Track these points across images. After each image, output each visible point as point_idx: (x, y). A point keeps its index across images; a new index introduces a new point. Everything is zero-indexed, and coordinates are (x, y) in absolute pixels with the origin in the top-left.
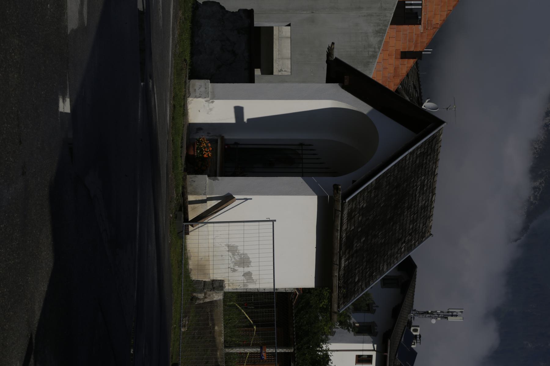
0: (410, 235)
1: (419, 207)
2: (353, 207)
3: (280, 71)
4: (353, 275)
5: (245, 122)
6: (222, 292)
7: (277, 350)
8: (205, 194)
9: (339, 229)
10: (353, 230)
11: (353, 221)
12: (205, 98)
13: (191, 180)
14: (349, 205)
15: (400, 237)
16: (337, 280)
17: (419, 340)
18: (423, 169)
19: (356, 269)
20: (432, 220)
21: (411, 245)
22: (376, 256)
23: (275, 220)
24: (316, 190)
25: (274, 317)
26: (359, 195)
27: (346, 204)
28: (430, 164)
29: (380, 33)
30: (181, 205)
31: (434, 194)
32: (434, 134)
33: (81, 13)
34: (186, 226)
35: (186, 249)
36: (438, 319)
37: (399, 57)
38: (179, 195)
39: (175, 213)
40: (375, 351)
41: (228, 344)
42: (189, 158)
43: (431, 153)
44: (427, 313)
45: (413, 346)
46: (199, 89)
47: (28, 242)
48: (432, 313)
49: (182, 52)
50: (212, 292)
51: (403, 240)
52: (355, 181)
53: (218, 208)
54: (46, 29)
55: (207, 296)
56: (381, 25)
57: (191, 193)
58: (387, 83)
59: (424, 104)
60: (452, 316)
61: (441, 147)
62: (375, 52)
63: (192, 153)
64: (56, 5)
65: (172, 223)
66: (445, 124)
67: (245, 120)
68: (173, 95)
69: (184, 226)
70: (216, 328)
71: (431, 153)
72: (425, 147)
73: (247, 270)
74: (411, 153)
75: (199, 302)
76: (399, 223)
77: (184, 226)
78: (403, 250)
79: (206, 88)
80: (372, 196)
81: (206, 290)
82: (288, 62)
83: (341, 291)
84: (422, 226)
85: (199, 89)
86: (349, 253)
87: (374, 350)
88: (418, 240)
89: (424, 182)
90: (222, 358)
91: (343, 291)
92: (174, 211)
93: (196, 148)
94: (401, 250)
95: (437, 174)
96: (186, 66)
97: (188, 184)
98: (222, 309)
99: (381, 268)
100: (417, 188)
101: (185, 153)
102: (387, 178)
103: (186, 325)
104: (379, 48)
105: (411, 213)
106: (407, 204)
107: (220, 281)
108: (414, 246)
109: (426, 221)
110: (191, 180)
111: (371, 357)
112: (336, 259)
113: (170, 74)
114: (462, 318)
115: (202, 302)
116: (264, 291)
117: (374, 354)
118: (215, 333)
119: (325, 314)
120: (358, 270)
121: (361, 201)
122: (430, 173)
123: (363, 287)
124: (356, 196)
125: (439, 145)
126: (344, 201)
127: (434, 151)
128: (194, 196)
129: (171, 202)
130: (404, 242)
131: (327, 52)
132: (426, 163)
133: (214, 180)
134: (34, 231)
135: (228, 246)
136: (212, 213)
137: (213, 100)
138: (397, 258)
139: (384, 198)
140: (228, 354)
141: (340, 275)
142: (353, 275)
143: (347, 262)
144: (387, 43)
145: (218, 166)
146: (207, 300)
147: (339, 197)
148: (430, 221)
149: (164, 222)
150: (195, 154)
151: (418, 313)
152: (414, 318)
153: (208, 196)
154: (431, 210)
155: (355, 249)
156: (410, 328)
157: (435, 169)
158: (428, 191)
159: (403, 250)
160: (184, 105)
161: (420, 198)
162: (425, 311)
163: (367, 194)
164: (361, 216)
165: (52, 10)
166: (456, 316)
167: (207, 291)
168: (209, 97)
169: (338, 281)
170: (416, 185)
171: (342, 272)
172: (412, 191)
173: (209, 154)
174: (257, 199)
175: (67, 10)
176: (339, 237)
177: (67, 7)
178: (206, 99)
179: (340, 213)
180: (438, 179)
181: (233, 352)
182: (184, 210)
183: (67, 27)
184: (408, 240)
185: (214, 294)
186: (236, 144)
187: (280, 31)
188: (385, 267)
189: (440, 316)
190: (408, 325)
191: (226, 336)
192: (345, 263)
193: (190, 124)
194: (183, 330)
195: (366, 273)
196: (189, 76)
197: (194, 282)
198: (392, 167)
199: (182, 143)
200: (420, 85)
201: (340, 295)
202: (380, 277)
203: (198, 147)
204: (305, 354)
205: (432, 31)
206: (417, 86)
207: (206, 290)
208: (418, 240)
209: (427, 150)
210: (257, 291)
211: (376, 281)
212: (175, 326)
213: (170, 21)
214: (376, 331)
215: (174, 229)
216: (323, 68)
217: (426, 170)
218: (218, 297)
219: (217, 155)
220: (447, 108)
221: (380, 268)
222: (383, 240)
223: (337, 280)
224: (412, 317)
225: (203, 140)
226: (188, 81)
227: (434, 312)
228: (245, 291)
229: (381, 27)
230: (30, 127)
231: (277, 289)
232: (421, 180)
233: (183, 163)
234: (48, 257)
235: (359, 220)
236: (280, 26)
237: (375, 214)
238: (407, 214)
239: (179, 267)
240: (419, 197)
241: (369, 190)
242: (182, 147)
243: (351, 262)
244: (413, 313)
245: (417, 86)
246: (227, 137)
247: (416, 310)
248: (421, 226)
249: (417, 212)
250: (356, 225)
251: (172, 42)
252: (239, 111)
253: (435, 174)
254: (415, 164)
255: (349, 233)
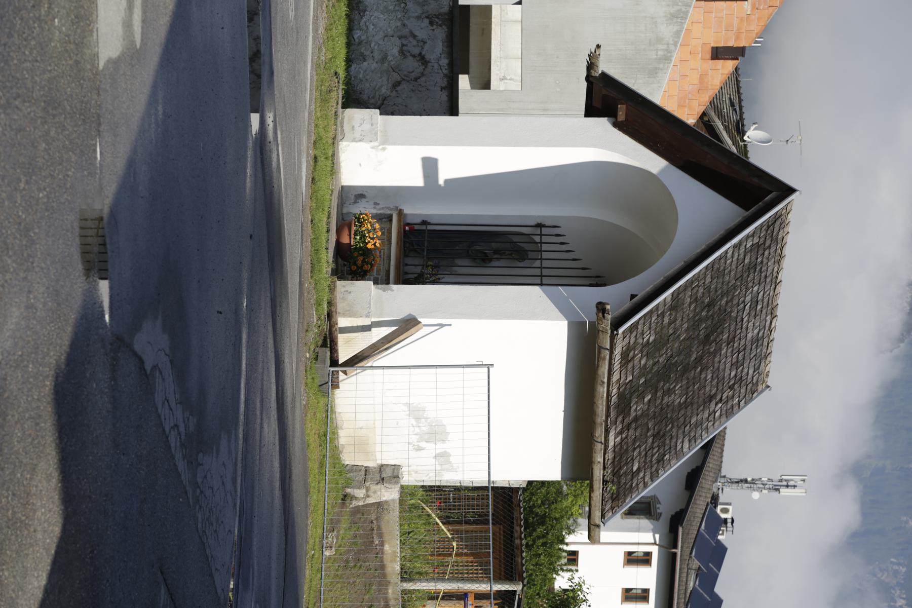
0: (731, 388)
1: (748, 339)
2: (632, 343)
3: (503, 79)
4: (630, 459)
5: (440, 185)
6: (397, 486)
7: (493, 586)
8: (368, 316)
9: (606, 380)
10: (630, 381)
11: (630, 365)
12: (371, 141)
13: (343, 290)
14: (624, 338)
15: (714, 392)
16: (600, 470)
17: (731, 526)
18: (756, 274)
19: (635, 449)
20: (770, 362)
21: (732, 407)
22: (670, 426)
23: (492, 365)
24: (565, 310)
25: (489, 509)
26: (642, 322)
27: (618, 337)
28: (769, 264)
29: (677, 18)
30: (326, 334)
31: (774, 317)
32: (778, 212)
33: (128, 25)
34: (335, 373)
35: (333, 412)
36: (764, 491)
37: (709, 56)
38: (323, 318)
39: (314, 349)
40: (657, 545)
41: (406, 575)
42: (341, 251)
43: (770, 245)
44: (746, 481)
45: (720, 537)
46: (359, 126)
47: (3, 500)
48: (753, 482)
49: (331, 59)
50: (379, 486)
51: (718, 398)
52: (637, 295)
53: (392, 341)
54: (49, 68)
55: (370, 493)
56: (680, 4)
57: (344, 314)
58: (687, 101)
59: (747, 134)
60: (787, 486)
61: (789, 235)
62: (668, 51)
63: (345, 240)
64: (73, 17)
65: (308, 369)
66: (797, 193)
67: (441, 182)
68: (313, 138)
69: (331, 372)
70: (387, 547)
71: (770, 245)
72: (760, 234)
73: (441, 447)
74: (735, 246)
75: (357, 504)
76: (712, 368)
77: (331, 374)
78: (717, 414)
79: (372, 125)
80: (664, 322)
81: (369, 483)
82: (518, 64)
83: (608, 489)
84: (752, 372)
85: (359, 126)
86: (622, 422)
87: (655, 544)
88: (745, 396)
89: (758, 297)
90: (396, 599)
91: (611, 489)
92: (312, 347)
93: (353, 232)
94: (715, 415)
95: (781, 281)
96: (337, 84)
97: (338, 297)
98: (397, 513)
99: (679, 447)
100: (745, 306)
101: (335, 240)
102: (692, 290)
103: (334, 546)
104: (675, 44)
105: (733, 350)
106: (727, 335)
107: (393, 467)
108: (737, 407)
109: (760, 364)
110: (343, 290)
111: (648, 554)
112: (599, 433)
113: (308, 103)
114: (804, 491)
115: (361, 503)
116: (471, 485)
117: (655, 550)
118: (385, 556)
119: (573, 484)
120: (638, 450)
121: (645, 330)
122: (768, 280)
123: (646, 480)
124: (637, 323)
125: (786, 230)
126: (615, 332)
127: (777, 242)
128: (350, 319)
129: (307, 331)
130: (721, 400)
131: (587, 61)
132: (762, 262)
133: (384, 291)
134: (19, 475)
135: (409, 405)
136: (381, 349)
137: (384, 146)
138: (707, 428)
139: (686, 326)
140: (405, 592)
141: (606, 460)
142: (630, 459)
143: (618, 437)
144: (688, 31)
145: (393, 262)
146: (370, 501)
147: (606, 324)
148: (767, 362)
149: (294, 372)
150: (352, 242)
151: (729, 481)
152: (722, 489)
153: (374, 320)
154: (768, 344)
155: (633, 414)
156: (716, 507)
157: (778, 273)
158: (764, 312)
159: (717, 414)
160: (333, 155)
161: (751, 324)
162: (742, 477)
163: (656, 319)
164: (645, 358)
165: (64, 29)
166: (795, 486)
167: (371, 486)
168: (377, 140)
169: (602, 472)
170: (744, 302)
171: (610, 455)
172: (736, 312)
173: (376, 242)
174: (461, 327)
175: (97, 23)
176: (605, 395)
177: (97, 17)
178: (372, 144)
179: (608, 352)
180: (782, 289)
181: (417, 588)
182: (331, 344)
183: (98, 57)
184: (727, 397)
185: (383, 491)
186: (424, 223)
187: (504, 10)
188: (686, 445)
189: (767, 486)
190: (713, 501)
191: (403, 558)
192: (615, 439)
193: (342, 187)
194: (327, 553)
195: (652, 456)
196: (343, 103)
197: (348, 468)
198: (701, 270)
199: (328, 223)
200: (740, 100)
201: (605, 494)
202: (677, 463)
203: (357, 230)
204: (540, 555)
205: (766, 11)
206: (736, 102)
207: (369, 483)
208: (745, 396)
209: (764, 239)
210: (459, 485)
211: (669, 469)
212: (313, 552)
213: (309, 7)
214: (658, 511)
215: (313, 378)
216: (578, 79)
217: (761, 275)
218: (389, 494)
219: (390, 244)
220: (787, 141)
221: (676, 446)
222: (683, 399)
223: (600, 470)
224: (719, 489)
225: (366, 218)
226: (340, 110)
227: (757, 480)
228: (438, 484)
229: (679, 8)
230: (12, 270)
231: (493, 482)
232: (752, 292)
233: (331, 259)
234: (49, 517)
235: (640, 363)
236: (503, 4)
237: (669, 354)
238: (727, 351)
239: (321, 445)
240: (748, 322)
241: (659, 312)
242: (328, 231)
243: (626, 437)
244: (721, 481)
245: (736, 102)
246: (408, 210)
247: (727, 476)
248: (751, 372)
249: (744, 349)
250: (635, 374)
251: (313, 43)
252: (430, 166)
253: (778, 282)
254: (742, 265)
255: (623, 388)
